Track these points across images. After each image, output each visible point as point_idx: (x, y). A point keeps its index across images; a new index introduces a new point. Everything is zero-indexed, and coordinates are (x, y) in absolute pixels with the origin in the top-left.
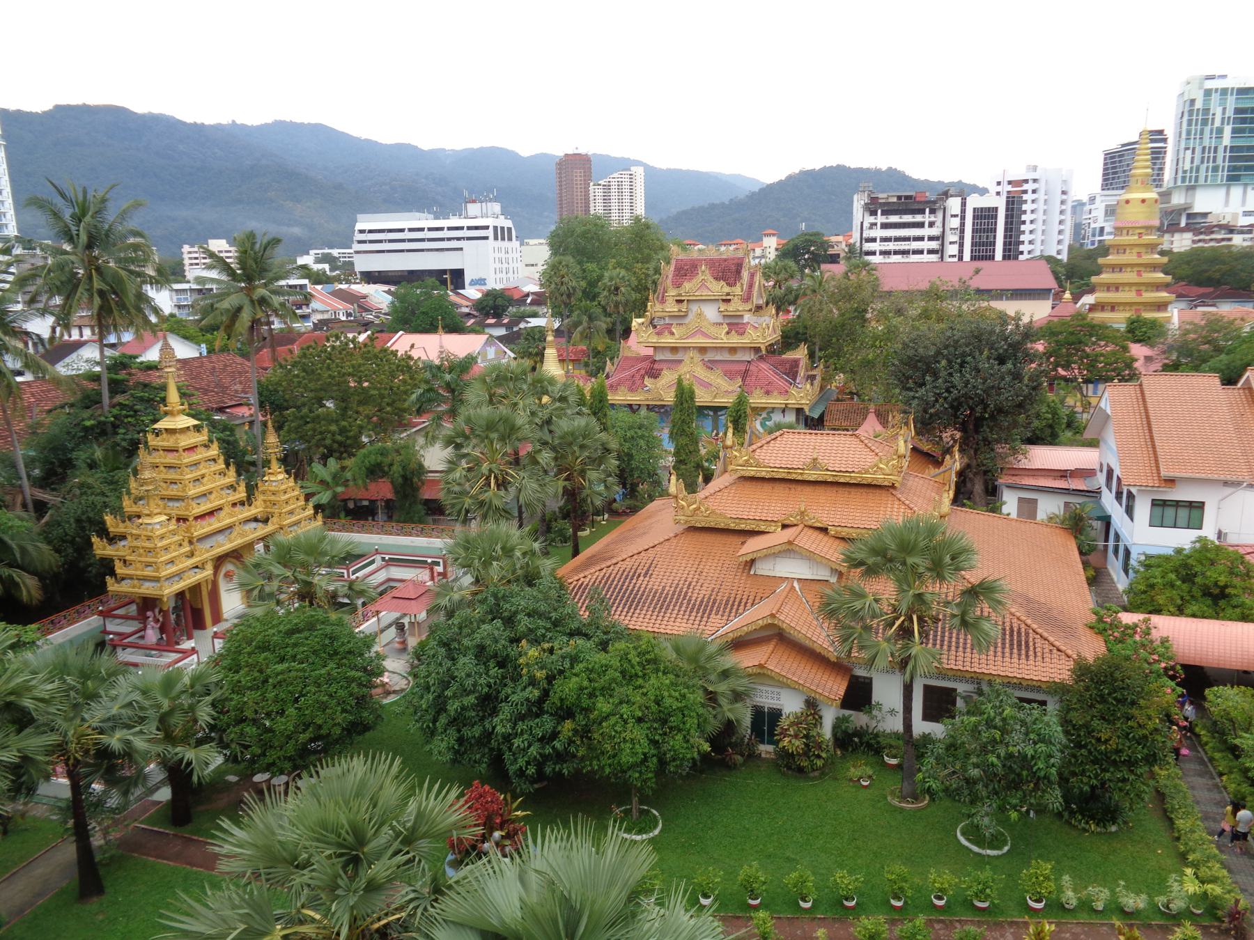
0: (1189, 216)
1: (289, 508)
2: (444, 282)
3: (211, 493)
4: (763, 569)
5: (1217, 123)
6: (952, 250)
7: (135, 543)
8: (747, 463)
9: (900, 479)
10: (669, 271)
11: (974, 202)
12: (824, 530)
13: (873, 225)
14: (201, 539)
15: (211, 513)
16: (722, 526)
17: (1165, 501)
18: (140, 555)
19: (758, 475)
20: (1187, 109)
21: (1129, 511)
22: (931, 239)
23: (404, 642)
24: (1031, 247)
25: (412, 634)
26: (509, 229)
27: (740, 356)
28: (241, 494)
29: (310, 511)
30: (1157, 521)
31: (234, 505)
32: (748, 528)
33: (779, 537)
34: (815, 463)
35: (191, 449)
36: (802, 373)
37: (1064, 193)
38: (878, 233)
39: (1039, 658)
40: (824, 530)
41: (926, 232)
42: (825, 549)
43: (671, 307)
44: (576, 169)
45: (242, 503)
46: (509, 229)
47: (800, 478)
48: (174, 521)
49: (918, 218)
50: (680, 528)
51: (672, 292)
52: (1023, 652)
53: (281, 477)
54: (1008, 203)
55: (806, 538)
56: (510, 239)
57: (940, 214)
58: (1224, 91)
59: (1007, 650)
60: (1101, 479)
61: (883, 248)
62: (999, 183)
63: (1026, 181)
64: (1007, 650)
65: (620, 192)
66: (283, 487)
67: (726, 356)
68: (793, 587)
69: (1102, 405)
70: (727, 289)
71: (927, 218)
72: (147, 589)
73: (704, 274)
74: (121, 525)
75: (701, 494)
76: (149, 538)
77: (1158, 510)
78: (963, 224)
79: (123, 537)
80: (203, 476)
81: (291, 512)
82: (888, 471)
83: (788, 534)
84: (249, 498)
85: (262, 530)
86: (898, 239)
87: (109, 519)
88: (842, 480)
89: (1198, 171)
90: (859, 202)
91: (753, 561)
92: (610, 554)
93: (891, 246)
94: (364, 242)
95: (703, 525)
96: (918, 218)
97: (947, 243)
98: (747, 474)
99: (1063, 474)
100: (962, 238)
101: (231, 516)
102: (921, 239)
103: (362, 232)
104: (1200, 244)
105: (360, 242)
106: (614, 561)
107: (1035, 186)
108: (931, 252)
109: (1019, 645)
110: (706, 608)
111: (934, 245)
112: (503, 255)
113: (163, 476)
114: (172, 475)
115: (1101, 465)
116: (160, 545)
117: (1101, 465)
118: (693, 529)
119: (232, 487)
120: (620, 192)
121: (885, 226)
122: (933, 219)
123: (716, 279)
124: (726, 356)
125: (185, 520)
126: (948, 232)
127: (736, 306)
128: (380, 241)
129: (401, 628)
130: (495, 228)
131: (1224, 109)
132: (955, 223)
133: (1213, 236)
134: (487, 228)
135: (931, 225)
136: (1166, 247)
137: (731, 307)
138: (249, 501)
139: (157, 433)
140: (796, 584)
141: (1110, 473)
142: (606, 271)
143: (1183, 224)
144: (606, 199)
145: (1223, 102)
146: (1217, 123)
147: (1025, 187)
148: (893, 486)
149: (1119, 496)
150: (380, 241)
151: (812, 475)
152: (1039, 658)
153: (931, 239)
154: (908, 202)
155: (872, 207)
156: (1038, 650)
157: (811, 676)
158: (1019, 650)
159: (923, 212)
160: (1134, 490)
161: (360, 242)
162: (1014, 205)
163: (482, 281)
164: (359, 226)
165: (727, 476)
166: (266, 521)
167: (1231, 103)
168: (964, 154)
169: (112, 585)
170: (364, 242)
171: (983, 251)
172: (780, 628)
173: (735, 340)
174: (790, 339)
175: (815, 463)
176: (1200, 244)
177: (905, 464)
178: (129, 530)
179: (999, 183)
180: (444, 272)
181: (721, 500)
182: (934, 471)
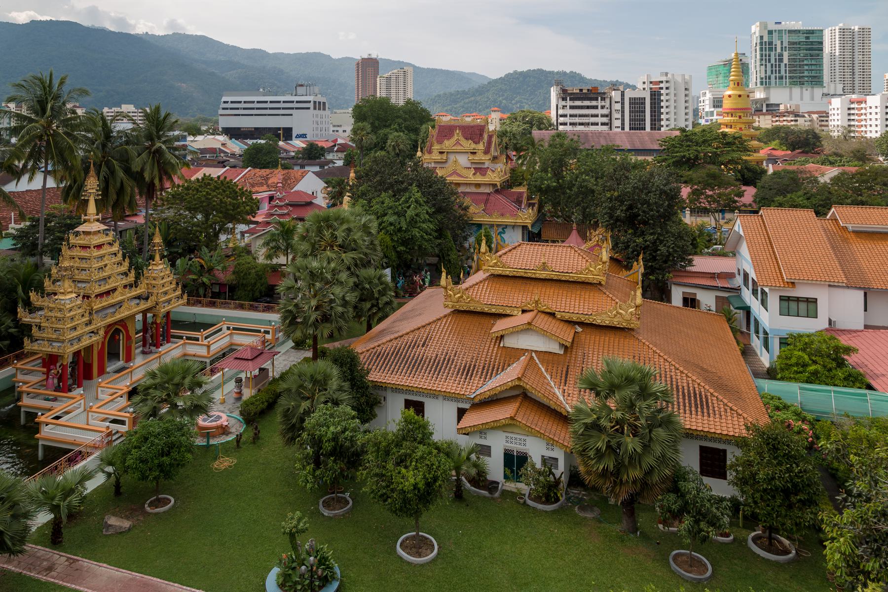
0: (768, 105)
1: (165, 289)
2: (278, 136)
3: (109, 278)
4: (511, 342)
5: (779, 50)
6: (617, 123)
7: (50, 314)
8: (496, 265)
9: (604, 279)
10: (433, 132)
11: (629, 94)
12: (552, 315)
13: (564, 107)
14: (97, 312)
15: (108, 293)
16: (479, 309)
17: (789, 297)
18: (52, 323)
19: (504, 273)
20: (759, 41)
21: (764, 303)
22: (603, 116)
23: (240, 393)
24: (668, 123)
25: (247, 386)
26: (324, 103)
27: (482, 190)
28: (132, 277)
29: (179, 292)
30: (785, 312)
31: (125, 287)
32: (497, 312)
33: (522, 319)
34: (544, 267)
35: (99, 247)
36: (525, 201)
37: (686, 89)
38: (569, 112)
39: (717, 416)
40: (552, 315)
41: (599, 111)
42: (551, 328)
43: (436, 156)
44: (369, 67)
45: (131, 286)
46: (324, 103)
47: (533, 276)
48: (80, 298)
49: (594, 103)
50: (448, 311)
51: (436, 147)
52: (705, 410)
53: (161, 267)
54: (651, 95)
55: (540, 320)
56: (324, 109)
57: (608, 101)
58: (780, 31)
59: (693, 409)
60: (739, 281)
61: (572, 121)
62: (644, 83)
63: (662, 82)
64: (693, 409)
65: (397, 82)
66: (162, 274)
67: (473, 190)
68: (532, 357)
69: (736, 228)
70: (473, 146)
71: (599, 103)
72: (55, 348)
73: (458, 135)
74: (41, 300)
75: (464, 286)
76: (60, 310)
77: (785, 304)
78: (623, 107)
79: (41, 309)
80: (106, 266)
81: (166, 293)
82: (595, 273)
83: (528, 317)
84: (136, 282)
85: (144, 306)
86: (581, 116)
87: (33, 295)
88: (563, 279)
89: (770, 78)
90: (554, 93)
91: (502, 337)
92: (397, 329)
93: (577, 120)
94: (227, 109)
95: (465, 308)
96: (594, 103)
97: (613, 119)
98: (496, 273)
99: (712, 276)
100: (623, 116)
101: (122, 294)
102: (597, 116)
103: (225, 102)
104: (777, 123)
105: (223, 109)
106: (400, 334)
107: (668, 85)
108: (603, 124)
109: (702, 405)
110: (468, 372)
111: (605, 120)
112: (319, 119)
113: (76, 265)
114: (84, 265)
115: (739, 270)
116: (68, 315)
117: (739, 270)
118: (457, 312)
119: (126, 274)
120: (397, 82)
121: (572, 107)
122: (603, 104)
123: (467, 139)
124: (473, 190)
125: (88, 297)
126: (613, 112)
127: (480, 157)
128: (238, 109)
129: (239, 381)
130: (315, 102)
131: (782, 42)
132: (618, 106)
133: (785, 118)
134: (310, 102)
135: (603, 107)
136: (756, 124)
137: (477, 158)
138: (135, 284)
139: (77, 234)
140: (534, 354)
141: (746, 276)
142: (391, 130)
143: (764, 111)
144: (388, 88)
145: (780, 38)
146: (779, 50)
147: (661, 85)
148: (600, 284)
149: (755, 292)
150: (238, 109)
151: (543, 275)
152: (717, 416)
153: (603, 116)
154: (586, 94)
155: (565, 95)
156: (716, 409)
157: (549, 427)
158: (702, 409)
159: (597, 99)
160: (766, 290)
161: (223, 109)
162: (655, 96)
163: (304, 136)
164: (224, 99)
165: (481, 272)
166: (147, 299)
167: (786, 39)
168: (623, 63)
169: (28, 345)
170: (227, 109)
171: (637, 124)
172: (524, 389)
173: (479, 179)
174: (514, 180)
175: (544, 267)
176: (777, 123)
177: (607, 266)
178: (46, 304)
179: (644, 83)
180: (279, 129)
181: (476, 289)
182: (625, 273)
